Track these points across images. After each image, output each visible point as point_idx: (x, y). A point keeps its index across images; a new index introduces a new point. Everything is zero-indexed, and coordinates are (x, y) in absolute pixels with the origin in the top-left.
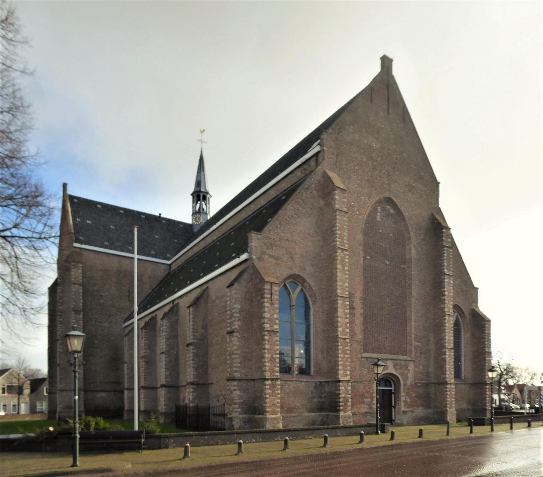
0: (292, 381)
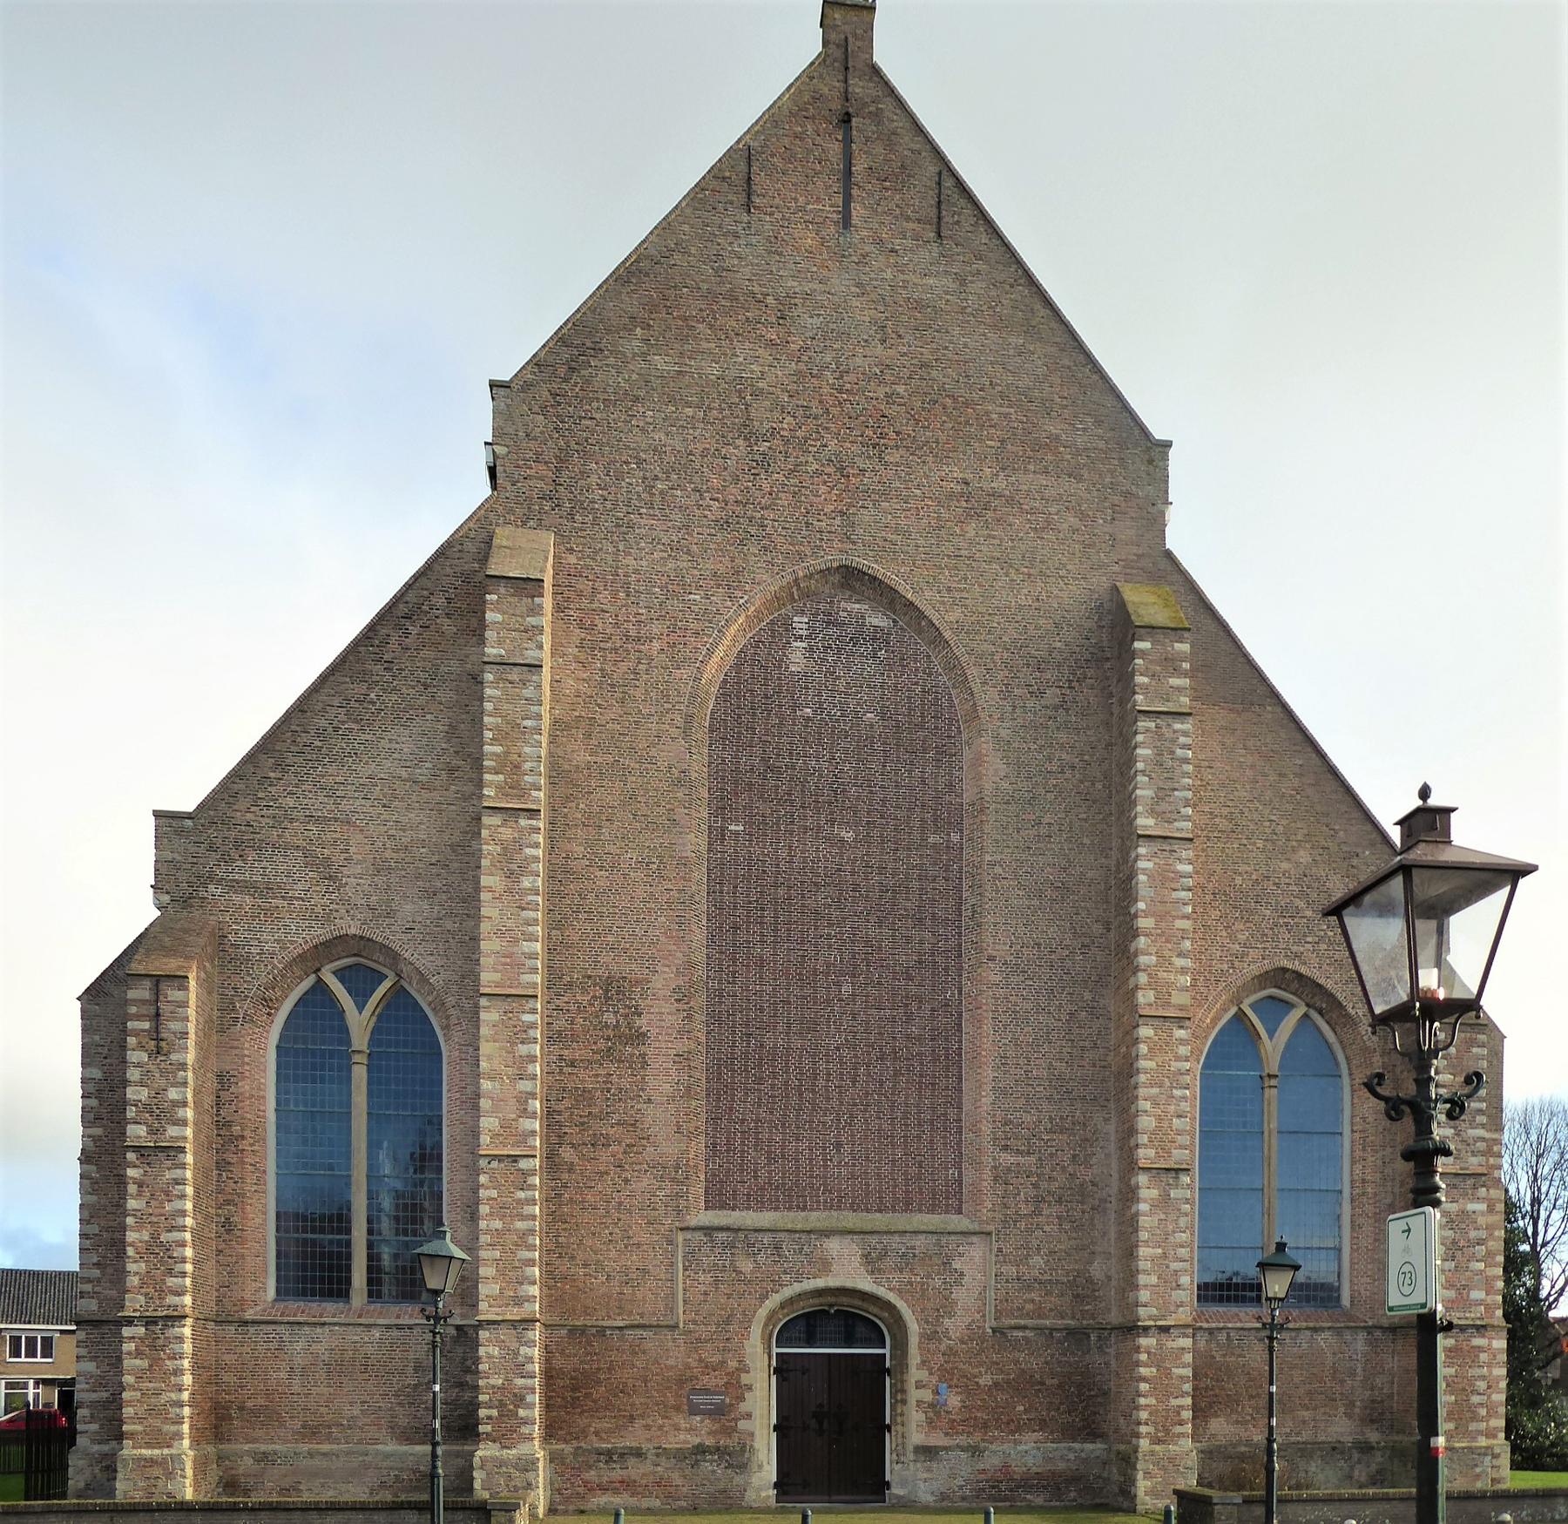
0: (324, 1324)
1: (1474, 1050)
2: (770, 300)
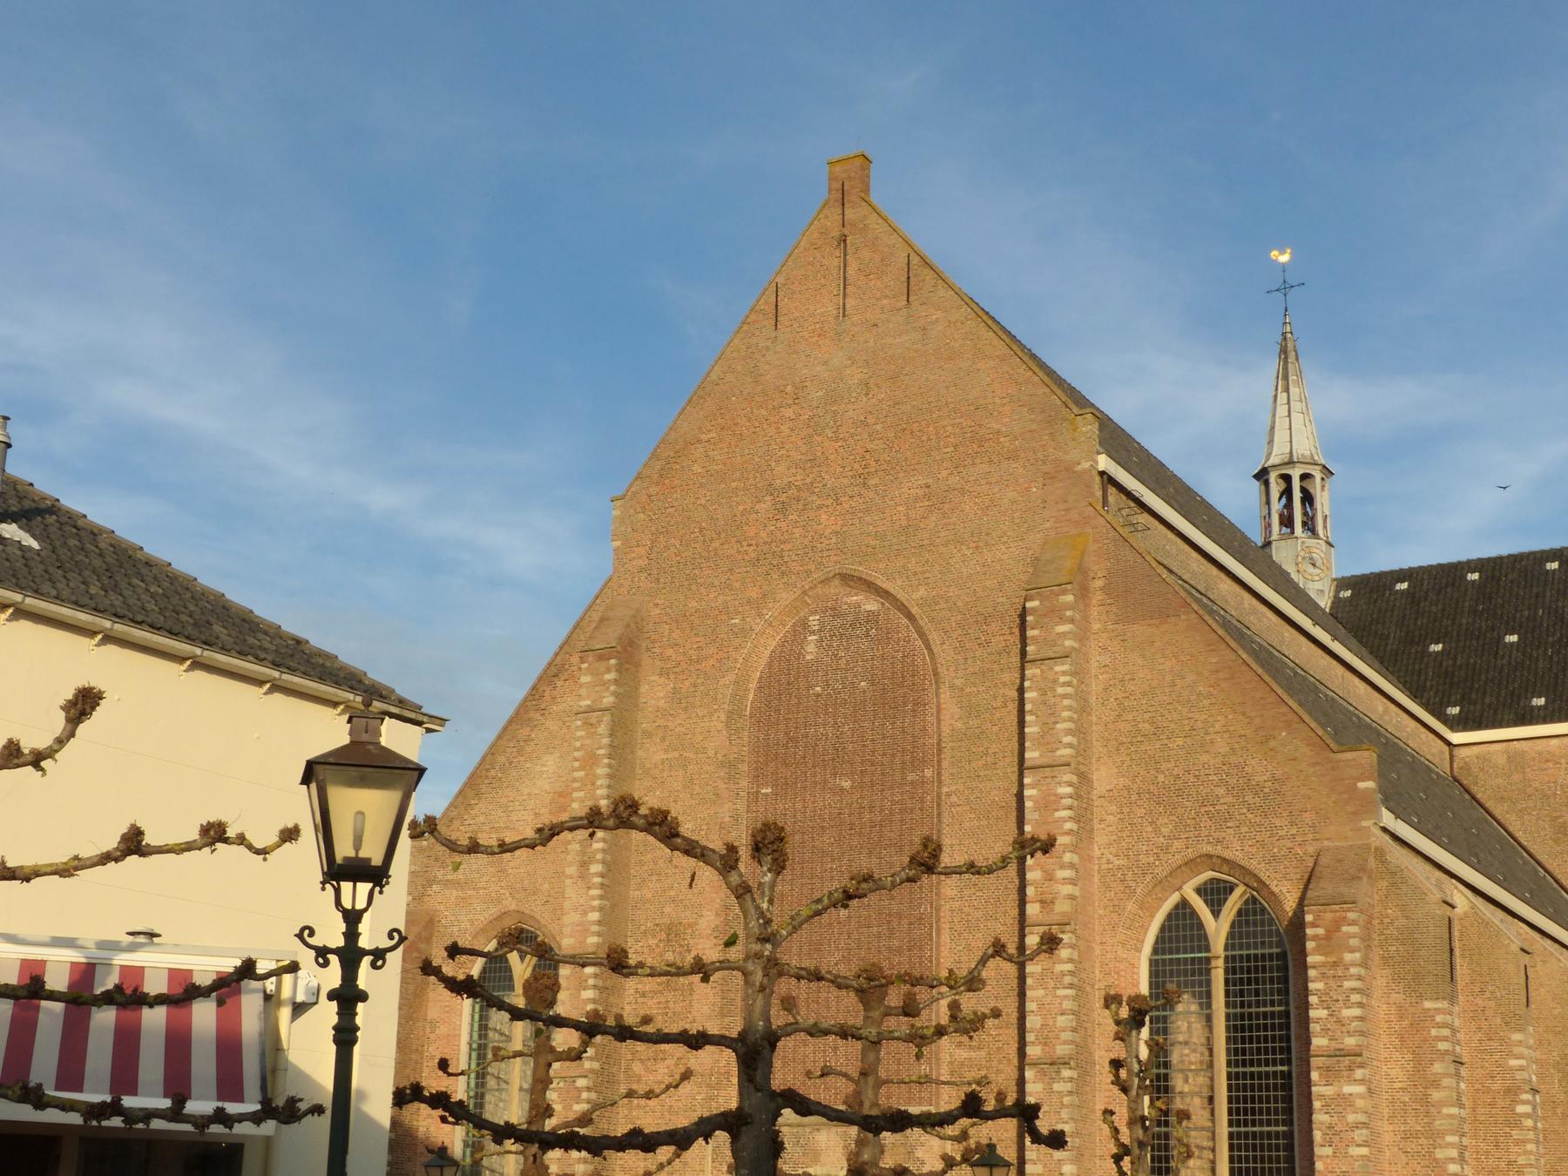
1: (1345, 929)
2: (789, 389)
